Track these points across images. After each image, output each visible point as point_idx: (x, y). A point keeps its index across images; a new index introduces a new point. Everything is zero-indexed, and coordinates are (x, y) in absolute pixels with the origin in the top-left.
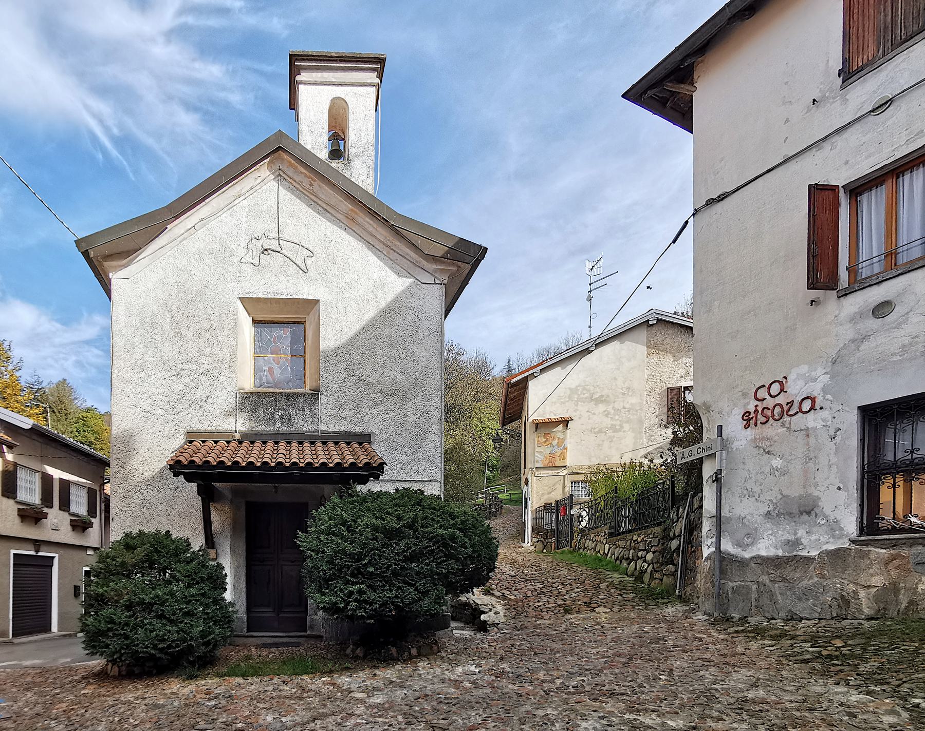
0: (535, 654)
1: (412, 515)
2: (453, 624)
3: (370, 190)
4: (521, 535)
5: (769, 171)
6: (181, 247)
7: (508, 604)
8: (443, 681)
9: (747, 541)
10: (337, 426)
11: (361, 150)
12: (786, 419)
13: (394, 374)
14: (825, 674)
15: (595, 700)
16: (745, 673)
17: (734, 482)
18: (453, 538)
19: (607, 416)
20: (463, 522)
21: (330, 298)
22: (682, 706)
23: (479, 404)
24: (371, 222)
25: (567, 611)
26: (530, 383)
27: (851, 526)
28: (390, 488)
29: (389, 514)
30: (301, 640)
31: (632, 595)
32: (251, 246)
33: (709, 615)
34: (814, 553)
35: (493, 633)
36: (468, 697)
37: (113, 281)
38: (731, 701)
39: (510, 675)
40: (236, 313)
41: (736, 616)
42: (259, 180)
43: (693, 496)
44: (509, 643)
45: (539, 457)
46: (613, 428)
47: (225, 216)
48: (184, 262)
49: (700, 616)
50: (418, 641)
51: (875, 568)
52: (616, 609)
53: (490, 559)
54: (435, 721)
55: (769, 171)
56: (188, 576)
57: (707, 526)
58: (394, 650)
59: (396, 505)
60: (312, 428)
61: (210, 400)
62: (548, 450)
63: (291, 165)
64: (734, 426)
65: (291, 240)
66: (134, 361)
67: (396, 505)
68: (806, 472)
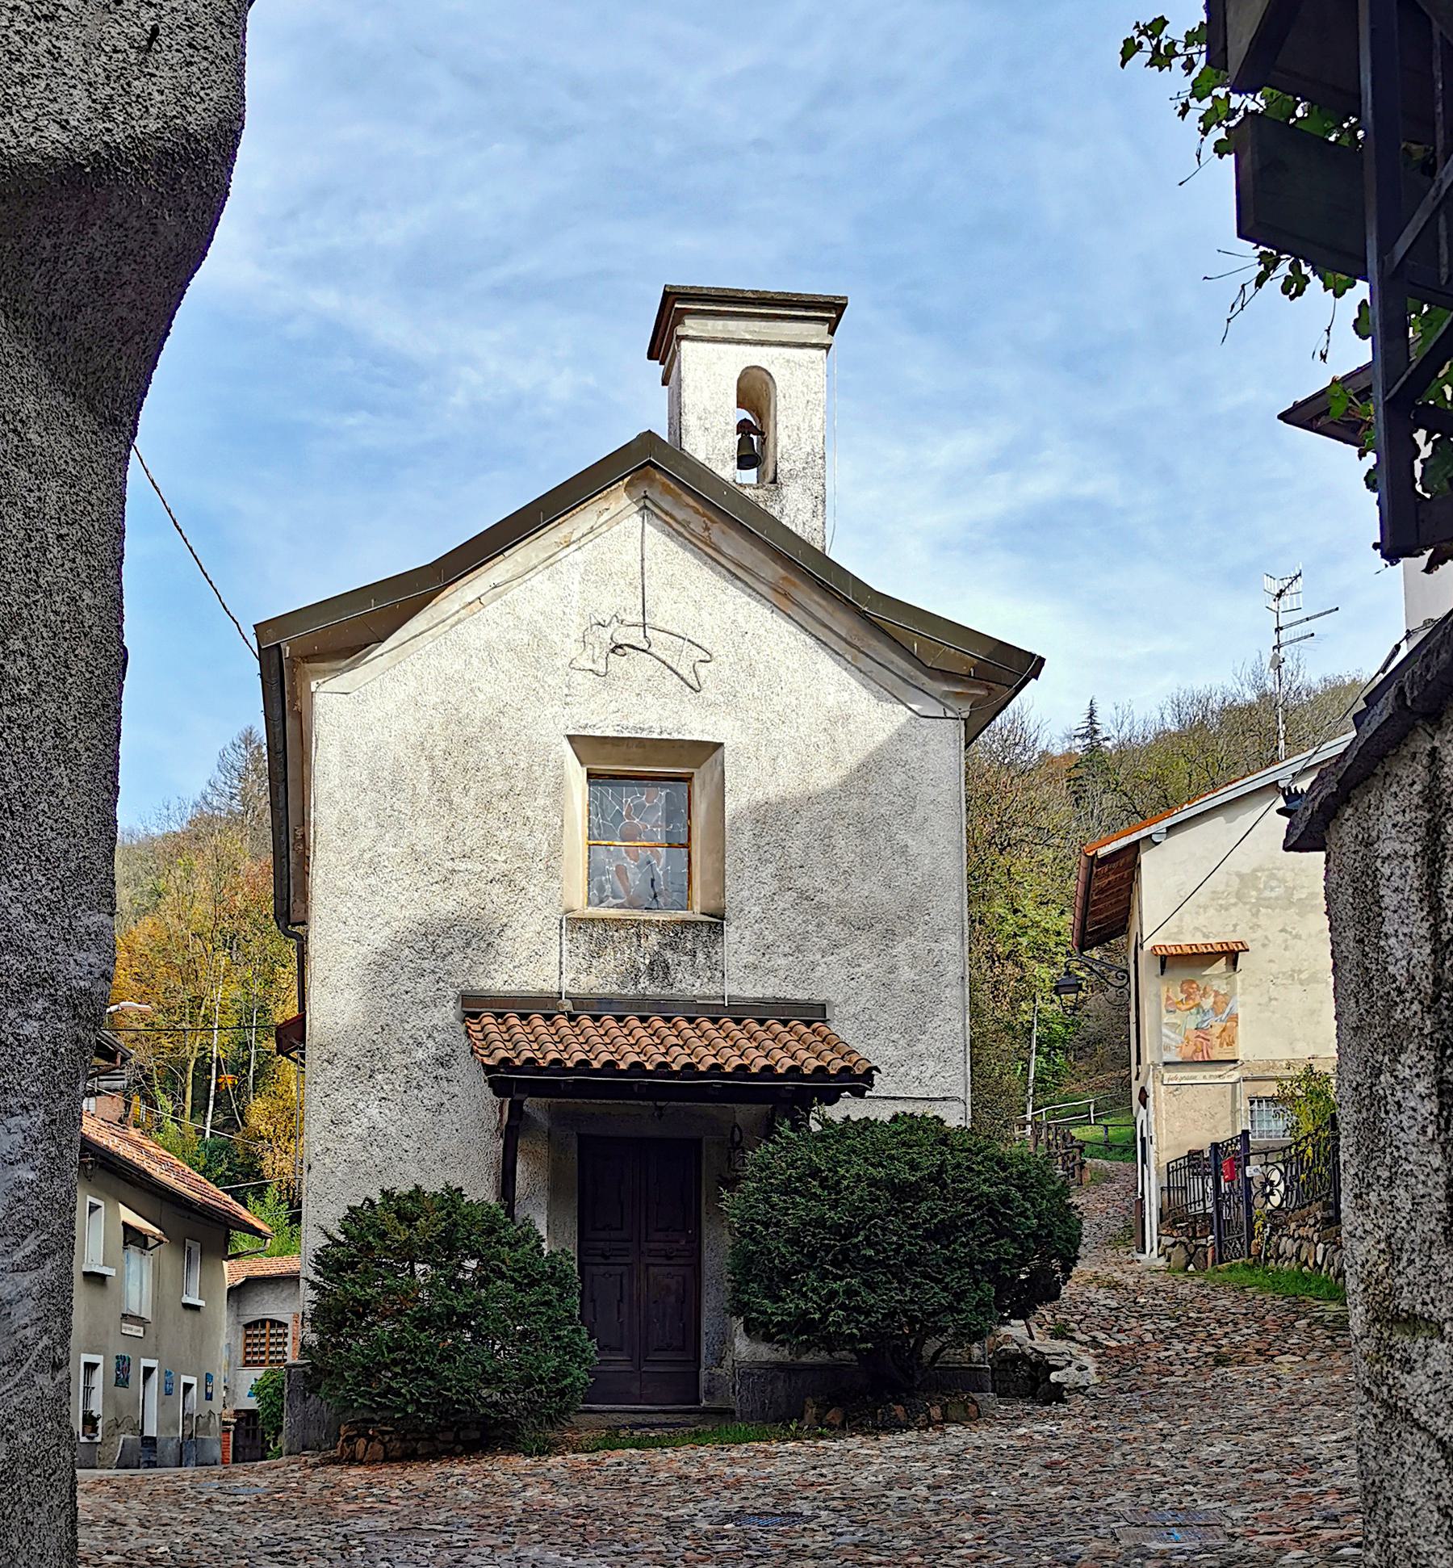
1: (937, 1160)
4: (1134, 1235)
6: (453, 636)
7: (1104, 1354)
10: (759, 987)
11: (799, 466)
13: (868, 889)
18: (1006, 1200)
20: (1021, 1175)
21: (744, 739)
24: (823, 603)
26: (1146, 858)
29: (892, 1158)
30: (691, 1418)
32: (590, 639)
37: (319, 699)
40: (561, 766)
42: (606, 516)
45: (1172, 1038)
47: (538, 580)
48: (459, 665)
56: (519, 1270)
58: (899, 1410)
59: (904, 1144)
60: (711, 990)
61: (509, 932)
62: (1192, 1021)
63: (666, 490)
65: (668, 628)
66: (356, 853)
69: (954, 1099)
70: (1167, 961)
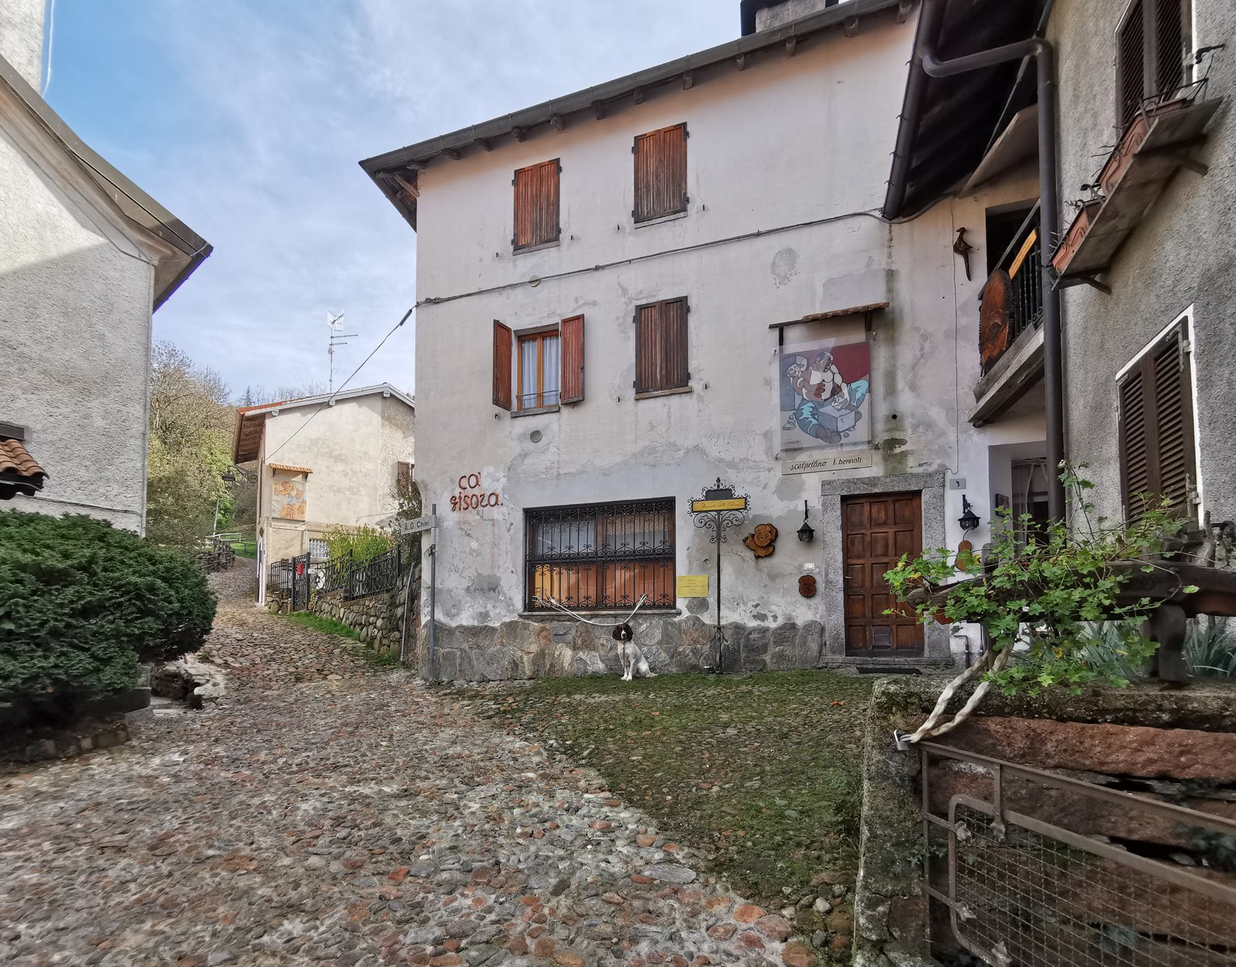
0: (259, 731)
2: (154, 701)
3: (34, 84)
5: (469, 295)
8: (129, 780)
9: (454, 611)
12: (480, 508)
14: (501, 727)
15: (319, 776)
16: (448, 733)
17: (445, 556)
18: (152, 589)
19: (345, 475)
20: (168, 570)
22: (398, 770)
23: (208, 432)
25: (299, 680)
26: (268, 422)
27: (519, 605)
28: (56, 513)
31: (363, 662)
33: (426, 680)
34: (497, 625)
35: (210, 710)
36: (163, 796)
38: (437, 759)
39: (225, 760)
41: (445, 680)
43: (415, 566)
44: (228, 720)
46: (350, 489)
49: (419, 681)
50: (95, 729)
51: (532, 639)
52: (347, 676)
53: (205, 618)
54: (107, 839)
55: (469, 295)
57: (424, 596)
58: (49, 745)
59: (63, 536)
62: (286, 500)
64: (444, 507)
67: (63, 536)
68: (493, 555)
69: (133, 513)
70: (275, 471)
